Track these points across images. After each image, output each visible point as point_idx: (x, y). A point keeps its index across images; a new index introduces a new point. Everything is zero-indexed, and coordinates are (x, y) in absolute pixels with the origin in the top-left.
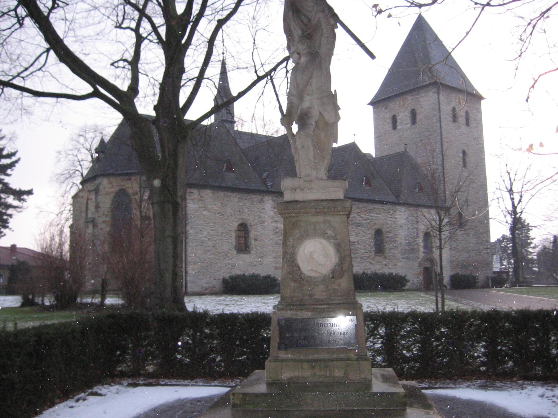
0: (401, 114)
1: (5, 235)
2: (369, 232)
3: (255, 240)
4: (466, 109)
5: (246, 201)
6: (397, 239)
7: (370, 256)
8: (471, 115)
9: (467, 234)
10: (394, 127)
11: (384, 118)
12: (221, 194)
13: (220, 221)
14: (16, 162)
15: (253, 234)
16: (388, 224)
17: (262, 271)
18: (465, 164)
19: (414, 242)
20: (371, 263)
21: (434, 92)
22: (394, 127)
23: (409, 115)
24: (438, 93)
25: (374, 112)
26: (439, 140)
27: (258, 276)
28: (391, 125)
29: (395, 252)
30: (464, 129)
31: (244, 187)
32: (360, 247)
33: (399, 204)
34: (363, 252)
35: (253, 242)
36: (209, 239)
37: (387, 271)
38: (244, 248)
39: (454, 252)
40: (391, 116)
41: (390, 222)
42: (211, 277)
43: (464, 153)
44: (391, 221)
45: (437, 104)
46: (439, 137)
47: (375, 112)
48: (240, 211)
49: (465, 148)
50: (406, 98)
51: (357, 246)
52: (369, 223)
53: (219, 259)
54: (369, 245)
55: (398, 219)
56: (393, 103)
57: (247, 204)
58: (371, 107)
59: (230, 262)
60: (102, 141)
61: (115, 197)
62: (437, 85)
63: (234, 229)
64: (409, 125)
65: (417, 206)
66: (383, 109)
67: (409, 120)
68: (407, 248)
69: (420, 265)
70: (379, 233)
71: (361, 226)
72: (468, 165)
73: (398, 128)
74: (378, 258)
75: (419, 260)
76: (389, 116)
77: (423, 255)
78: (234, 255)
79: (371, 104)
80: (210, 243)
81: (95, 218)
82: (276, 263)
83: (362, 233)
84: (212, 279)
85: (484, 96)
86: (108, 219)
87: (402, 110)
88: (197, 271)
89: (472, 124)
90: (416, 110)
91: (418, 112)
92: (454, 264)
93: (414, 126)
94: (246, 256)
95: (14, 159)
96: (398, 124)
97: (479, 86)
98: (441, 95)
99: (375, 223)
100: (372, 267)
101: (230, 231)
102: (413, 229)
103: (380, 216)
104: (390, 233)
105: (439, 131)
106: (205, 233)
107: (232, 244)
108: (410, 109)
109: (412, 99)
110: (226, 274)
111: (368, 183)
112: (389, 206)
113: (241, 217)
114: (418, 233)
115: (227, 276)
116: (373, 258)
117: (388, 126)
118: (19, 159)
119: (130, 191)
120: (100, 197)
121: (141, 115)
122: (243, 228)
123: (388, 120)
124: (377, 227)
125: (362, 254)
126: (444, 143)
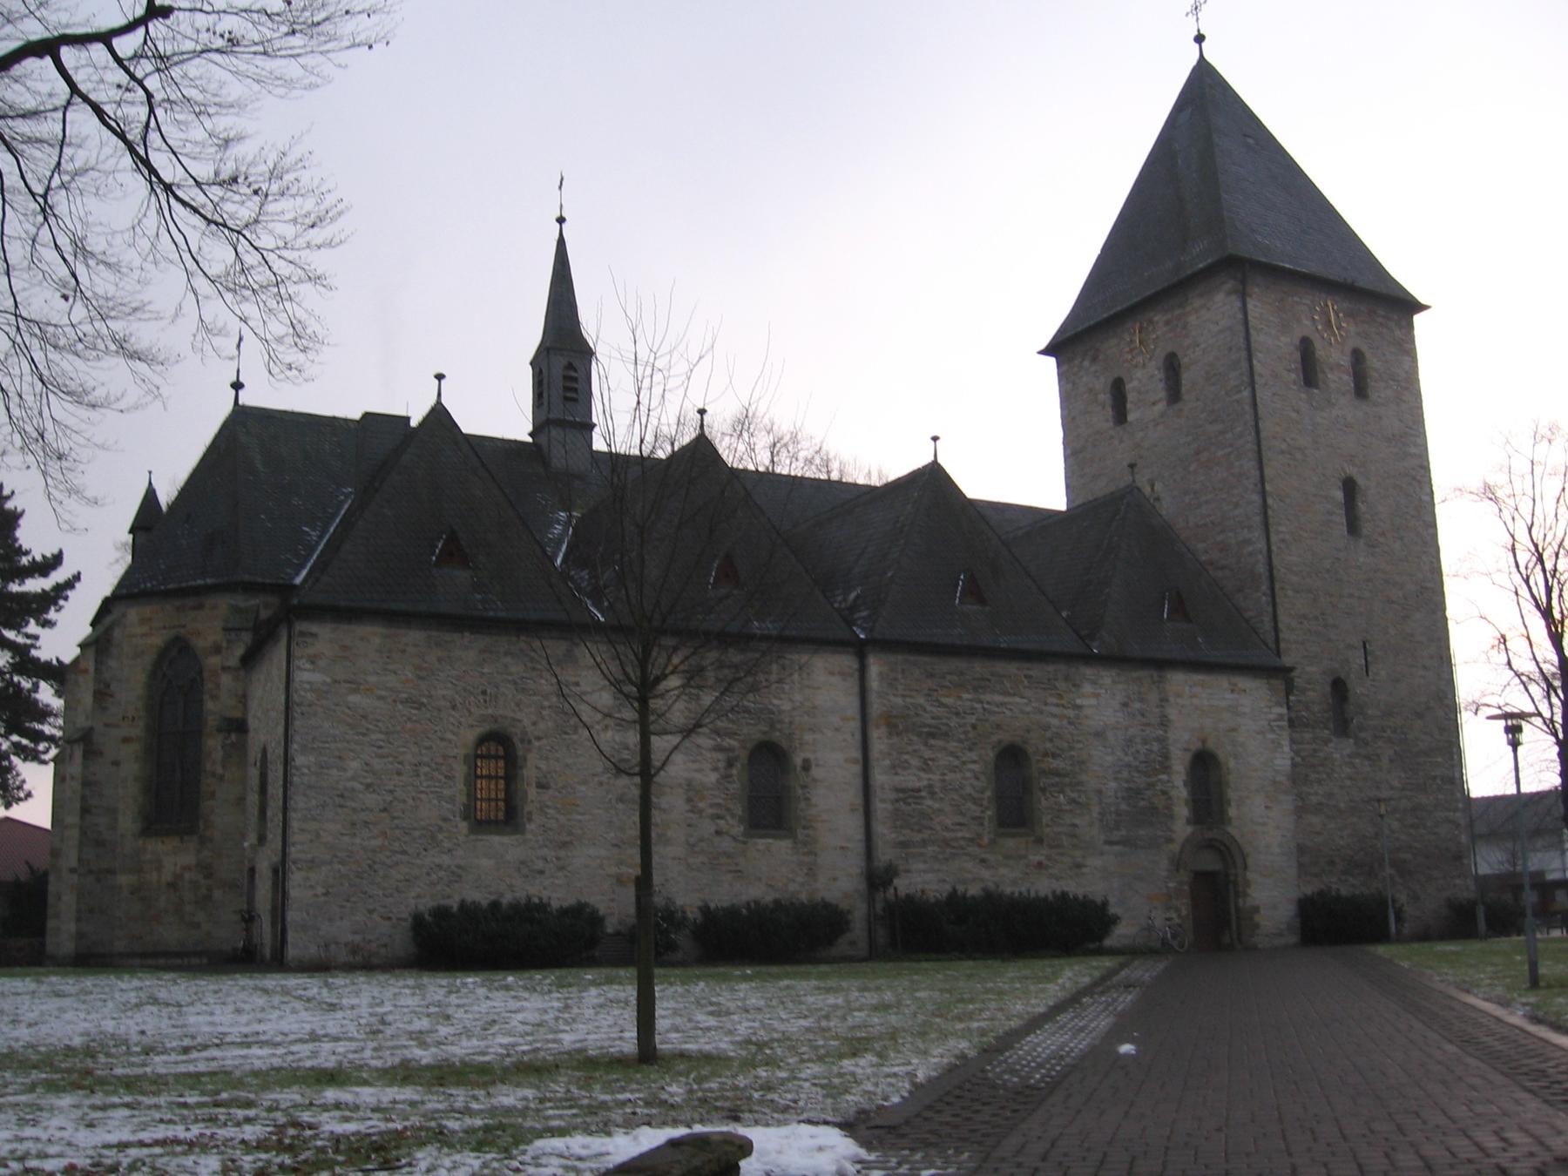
0: (1139, 374)
1: (29, 795)
2: (973, 756)
3: (542, 786)
4: (1351, 344)
5: (508, 660)
6: (1084, 777)
7: (980, 836)
8: (1373, 362)
9: (1368, 758)
10: (1120, 416)
11: (1091, 390)
12: (414, 636)
13: (409, 725)
14: (70, 584)
15: (532, 768)
16: (1047, 727)
17: (557, 893)
18: (1353, 527)
19: (1151, 786)
20: (983, 861)
21: (1229, 294)
22: (1120, 416)
23: (1160, 375)
24: (1244, 296)
25: (1060, 375)
26: (1249, 446)
27: (542, 907)
28: (1109, 412)
29: (1077, 821)
30: (1346, 408)
31: (502, 614)
32: (937, 806)
33: (1088, 659)
34: (948, 822)
35: (532, 792)
36: (368, 786)
37: (1043, 887)
38: (501, 816)
39: (1315, 820)
40: (1110, 380)
41: (1055, 722)
42: (371, 912)
43: (1349, 486)
44: (1061, 717)
45: (1242, 328)
46: (1251, 438)
47: (1062, 376)
48: (484, 693)
49: (1351, 471)
50: (1151, 322)
51: (929, 802)
52: (974, 727)
53: (404, 852)
54: (975, 801)
55: (1088, 712)
56: (1113, 342)
57: (513, 669)
58: (1051, 362)
59: (446, 860)
60: (150, 496)
61: (157, 664)
62: (1239, 269)
63: (461, 752)
64: (1161, 406)
65: (1162, 665)
66: (1086, 363)
67: (1160, 392)
68: (1123, 807)
69: (1177, 864)
70: (1012, 757)
71: (946, 735)
72: (1366, 529)
73: (1131, 417)
74: (1010, 843)
75: (1176, 847)
76: (1102, 384)
77: (1189, 829)
78: (461, 838)
79: (1048, 351)
80: (371, 799)
81: (91, 729)
82: (620, 863)
83: (945, 760)
84: (375, 916)
85: (1423, 301)
86: (137, 730)
87: (1140, 359)
88: (320, 890)
89: (1380, 391)
90: (1180, 354)
91: (1186, 360)
92: (1306, 856)
93: (1177, 407)
94: (506, 839)
95: (59, 576)
96: (1129, 406)
97: (1402, 264)
98: (1251, 304)
99: (998, 727)
100: (986, 874)
101: (445, 757)
102: (1145, 742)
103: (1018, 700)
104: (1054, 756)
105: (1249, 417)
106: (354, 765)
107: (452, 800)
108: (1161, 354)
109: (1167, 323)
110: (421, 898)
111: (975, 592)
112: (1051, 668)
113: (490, 711)
114: (1166, 756)
115: (426, 904)
116: (993, 842)
117: (1102, 418)
118: (77, 577)
119: (200, 644)
120: (113, 663)
121: (972, 503)
122: (500, 747)
123: (1101, 397)
124: (1006, 737)
125: (947, 829)
126: (1266, 454)
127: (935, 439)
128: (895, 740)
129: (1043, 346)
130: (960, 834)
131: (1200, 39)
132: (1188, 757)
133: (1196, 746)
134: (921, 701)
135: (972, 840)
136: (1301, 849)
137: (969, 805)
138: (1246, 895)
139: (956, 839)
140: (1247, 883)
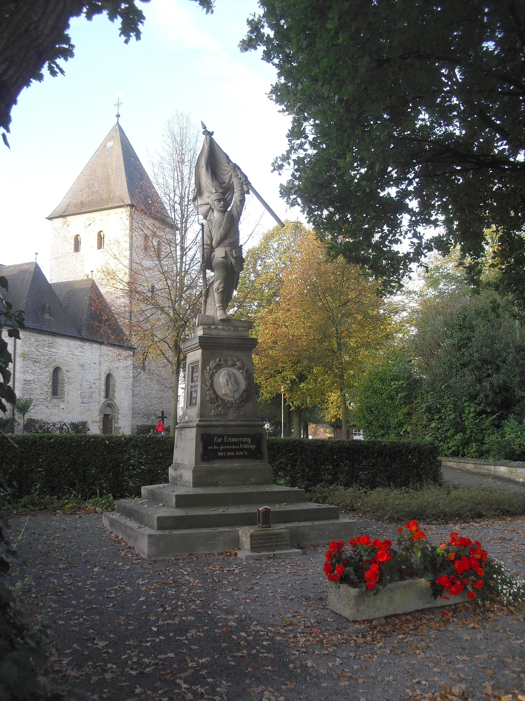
10: (77, 248)
24: (241, 246)
34: (38, 392)
51: (33, 385)
92: (135, 413)
124: (56, 364)
125: (38, 395)
127: (37, 254)
128: (25, 362)
129: (47, 216)
130: (41, 397)
131: (118, 116)
132: (106, 375)
133: (108, 372)
134: (33, 349)
135: (44, 399)
136: (133, 409)
137: (45, 387)
138: (118, 423)
139: (40, 399)
140: (118, 419)
